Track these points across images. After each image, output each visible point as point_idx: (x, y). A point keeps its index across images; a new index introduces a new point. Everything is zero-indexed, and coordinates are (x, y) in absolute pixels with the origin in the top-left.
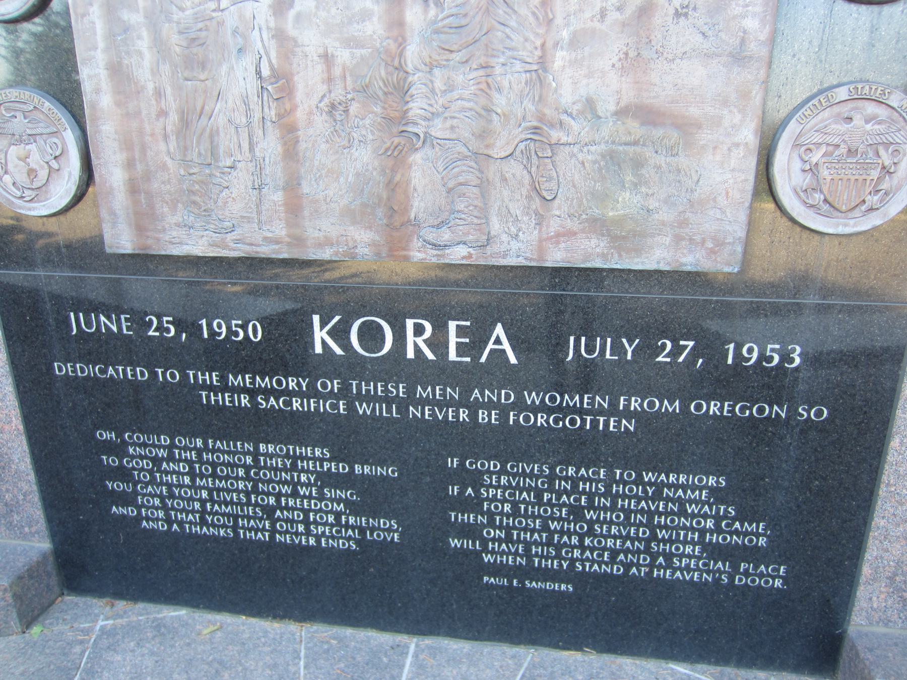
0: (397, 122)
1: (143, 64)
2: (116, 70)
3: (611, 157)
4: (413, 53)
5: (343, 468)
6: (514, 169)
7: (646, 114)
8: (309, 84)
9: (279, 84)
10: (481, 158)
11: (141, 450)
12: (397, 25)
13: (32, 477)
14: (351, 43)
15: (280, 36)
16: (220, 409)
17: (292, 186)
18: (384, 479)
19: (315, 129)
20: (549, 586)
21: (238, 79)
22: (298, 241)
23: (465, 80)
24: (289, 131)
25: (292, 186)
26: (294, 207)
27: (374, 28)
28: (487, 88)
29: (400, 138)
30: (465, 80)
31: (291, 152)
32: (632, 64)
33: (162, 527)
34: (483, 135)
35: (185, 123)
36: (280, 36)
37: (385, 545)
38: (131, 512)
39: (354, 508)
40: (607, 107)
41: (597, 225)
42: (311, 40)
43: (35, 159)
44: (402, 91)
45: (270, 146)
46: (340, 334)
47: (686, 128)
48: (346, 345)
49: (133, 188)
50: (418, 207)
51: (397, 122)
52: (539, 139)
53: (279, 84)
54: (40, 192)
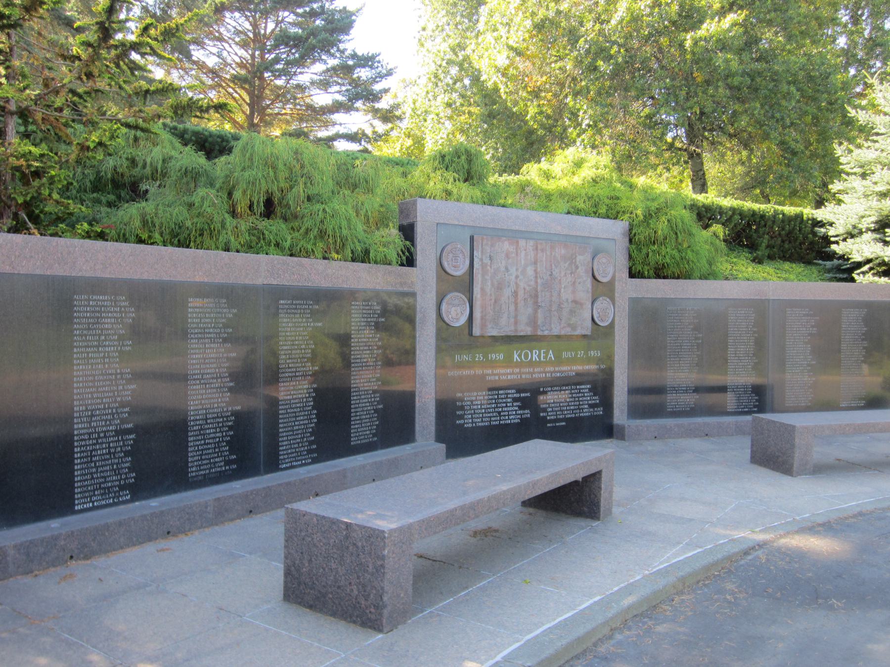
0: (536, 303)
1: (488, 288)
2: (482, 289)
3: (571, 311)
4: (539, 288)
5: (518, 395)
6: (556, 313)
7: (575, 302)
8: (521, 294)
9: (515, 294)
10: (550, 311)
11: (335, 143)
12: (537, 282)
13: (434, 415)
14: (529, 286)
15: (516, 283)
16: (297, 299)
17: (516, 317)
18: (527, 397)
19: (521, 304)
20: (466, 372)
21: (507, 292)
22: (516, 330)
23: (548, 294)
24: (516, 304)
25: (516, 317)
26: (516, 323)
27: (532, 283)
28: (551, 296)
29: (536, 306)
30: (548, 294)
31: (516, 309)
32: (574, 292)
33: (470, 425)
34: (551, 306)
35: (495, 302)
36: (516, 283)
37: (527, 418)
38: (462, 422)
39: (520, 408)
40: (570, 301)
41: (569, 325)
42: (522, 285)
43: (459, 311)
44: (536, 296)
45: (512, 308)
46: (520, 356)
47: (581, 304)
48: (521, 359)
49: (482, 318)
50: (539, 323)
51: (536, 303)
52: (560, 308)
53: (515, 294)
54: (458, 319)
